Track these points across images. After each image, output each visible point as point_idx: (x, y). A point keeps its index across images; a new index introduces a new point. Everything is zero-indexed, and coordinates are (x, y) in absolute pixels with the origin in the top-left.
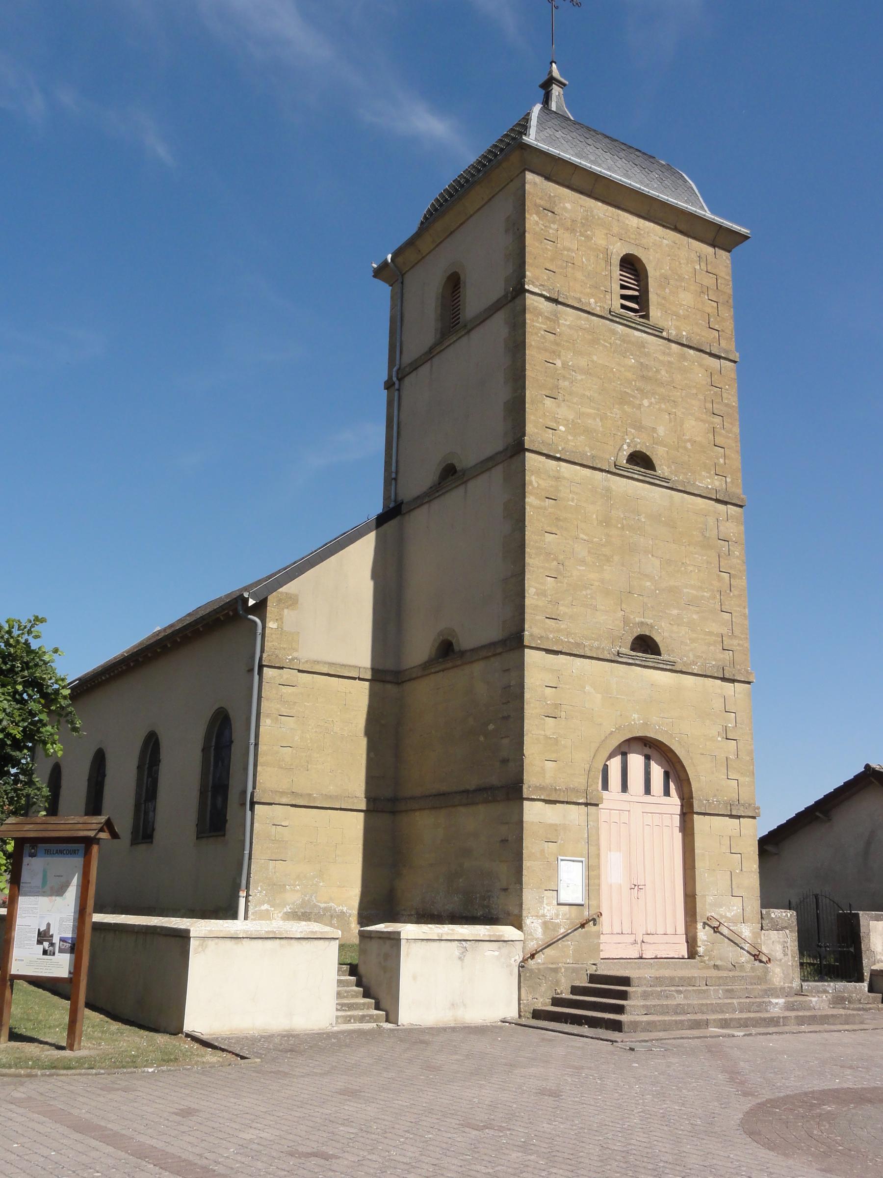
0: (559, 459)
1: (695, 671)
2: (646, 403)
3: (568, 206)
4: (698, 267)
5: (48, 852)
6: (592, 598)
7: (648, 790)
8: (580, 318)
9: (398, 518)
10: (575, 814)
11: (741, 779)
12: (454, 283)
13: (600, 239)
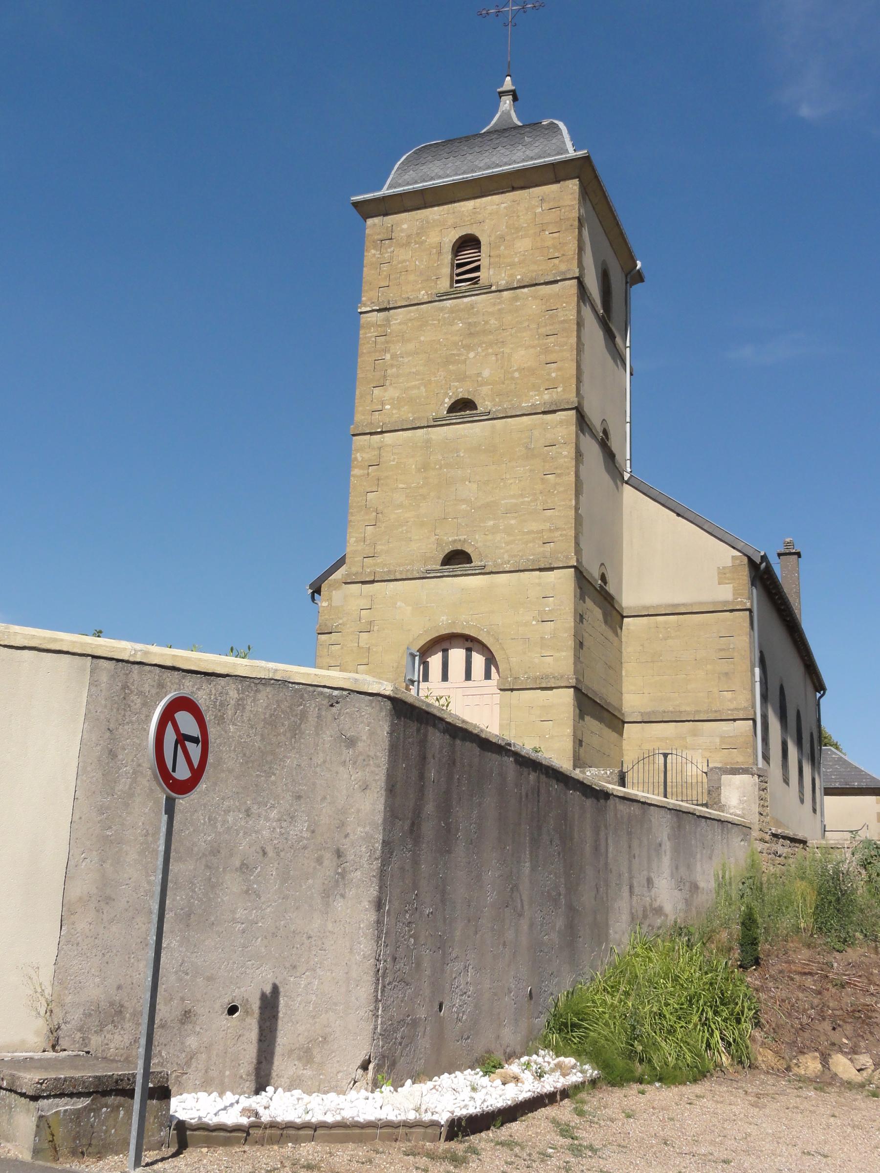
0: (382, 432)
1: (507, 569)
3: (405, 226)
6: (407, 532)
7: (468, 676)
8: (410, 312)
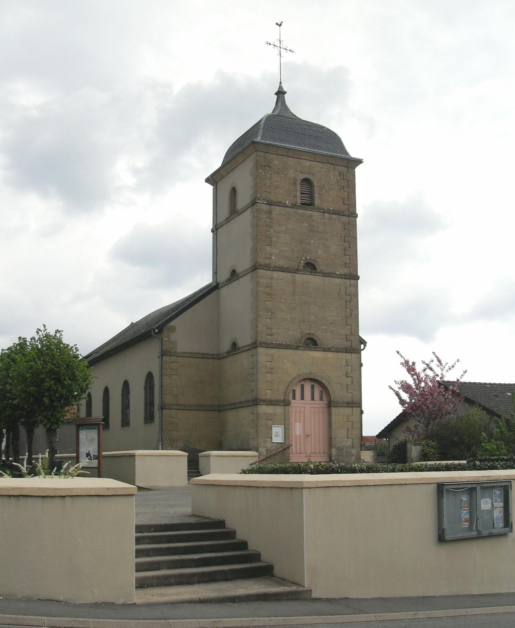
2: (312, 241)
4: (339, 178)
5: (87, 429)
7: (313, 399)
9: (217, 290)
10: (279, 410)
11: (354, 393)
12: (234, 191)
13: (291, 174)
